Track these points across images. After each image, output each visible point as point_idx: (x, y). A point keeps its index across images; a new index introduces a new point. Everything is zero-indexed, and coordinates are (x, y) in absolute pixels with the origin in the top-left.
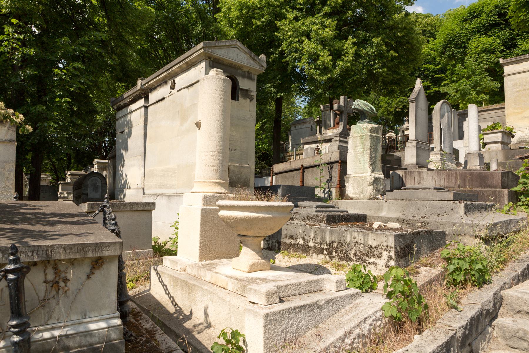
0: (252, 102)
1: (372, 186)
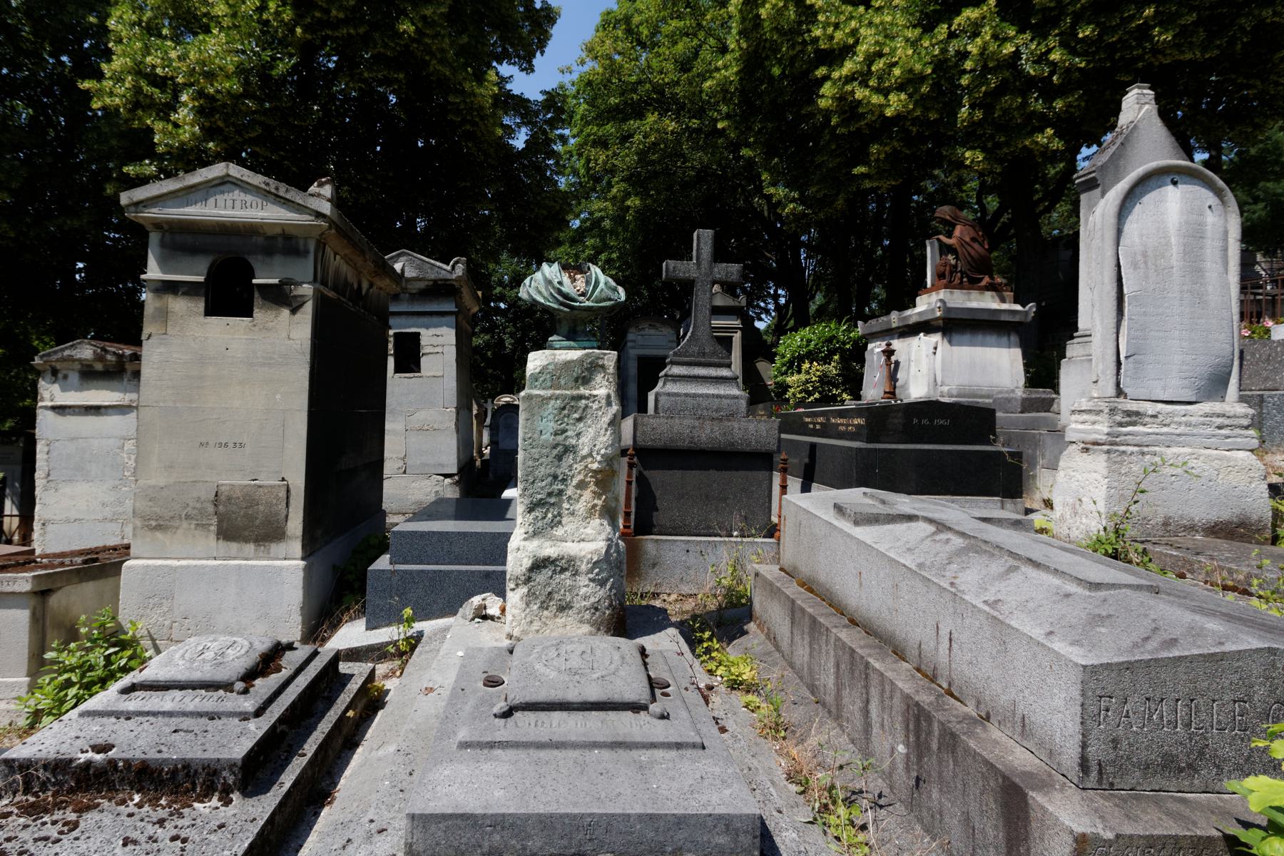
0: (298, 316)
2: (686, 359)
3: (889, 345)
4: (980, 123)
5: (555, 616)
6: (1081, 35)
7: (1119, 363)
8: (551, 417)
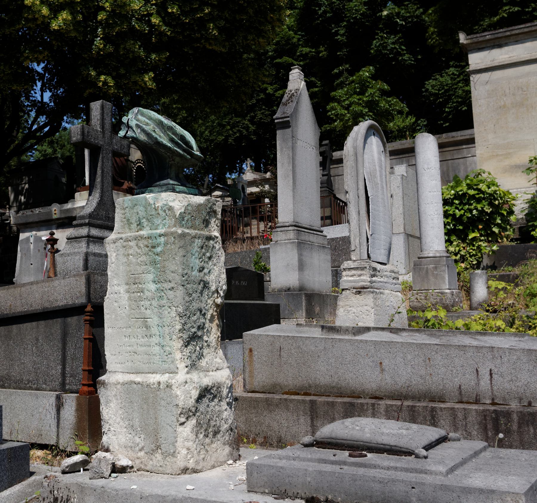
2: (99, 222)
3: (52, 234)
4: (109, 55)
5: (212, 442)
6: (170, 10)
7: (368, 239)
8: (197, 254)
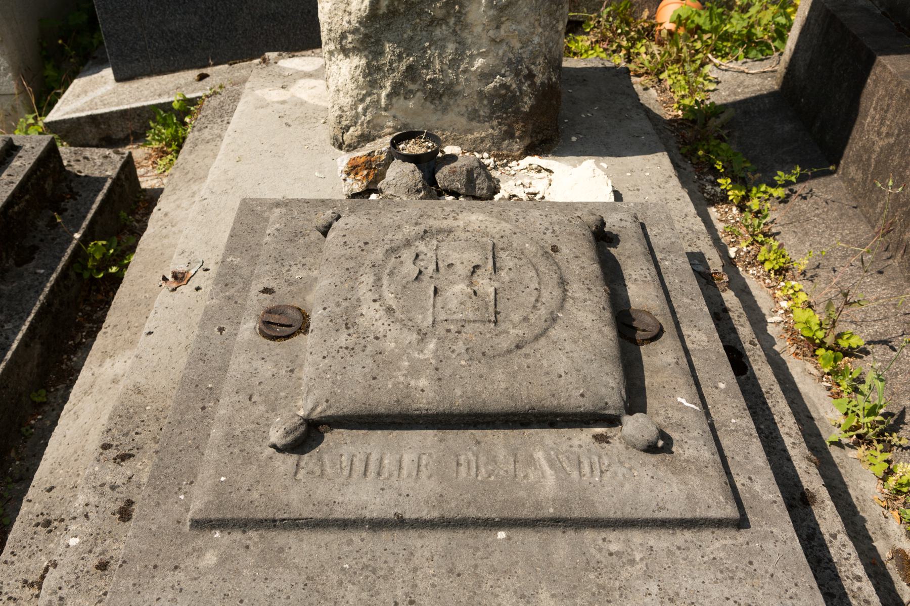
1: (358, 61)
